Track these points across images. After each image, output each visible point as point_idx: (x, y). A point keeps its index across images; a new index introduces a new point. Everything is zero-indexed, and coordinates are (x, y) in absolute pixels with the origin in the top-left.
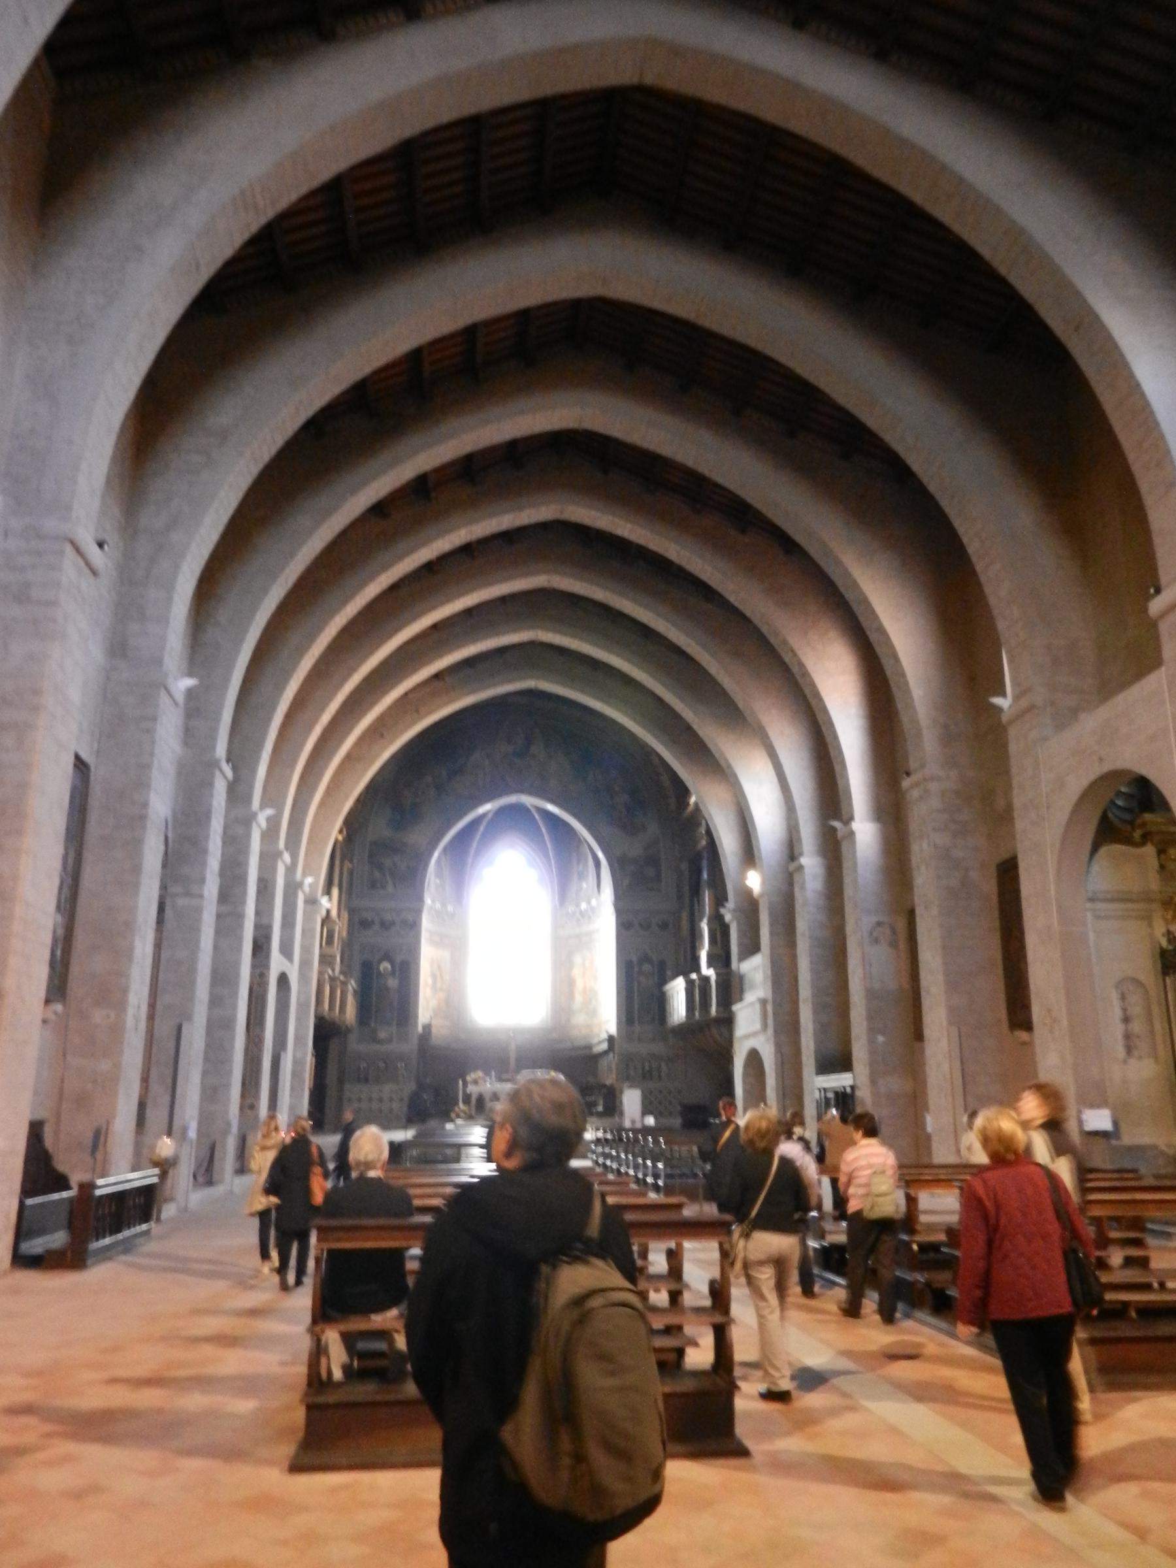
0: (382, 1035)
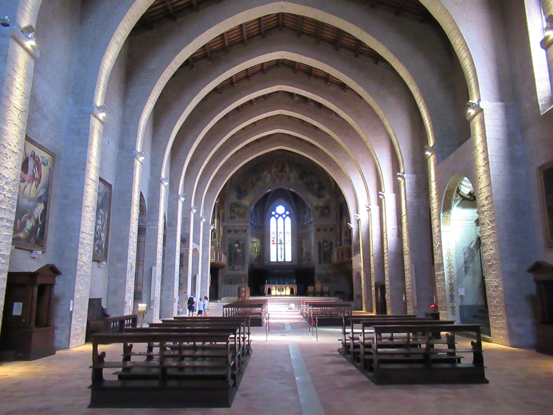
0: (236, 268)
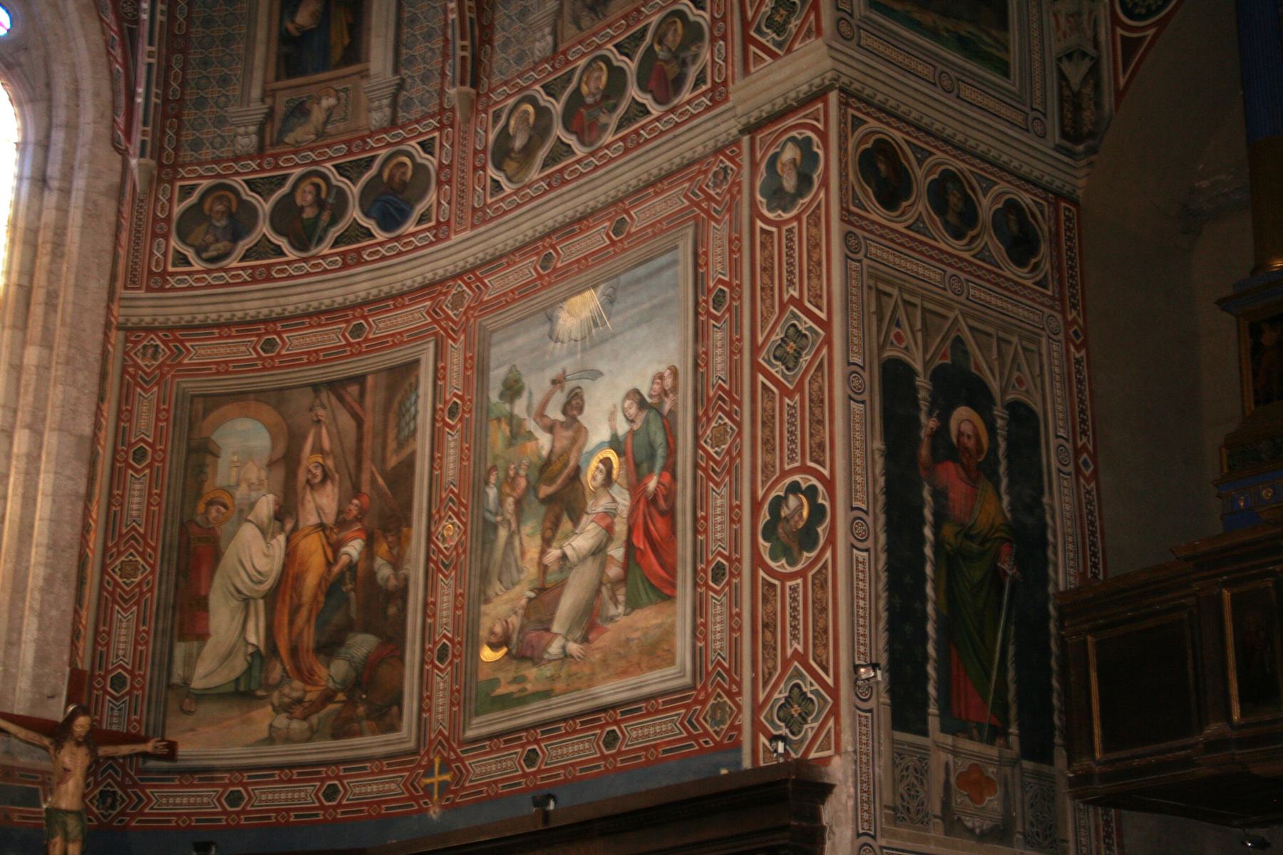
0: (59, 367)
